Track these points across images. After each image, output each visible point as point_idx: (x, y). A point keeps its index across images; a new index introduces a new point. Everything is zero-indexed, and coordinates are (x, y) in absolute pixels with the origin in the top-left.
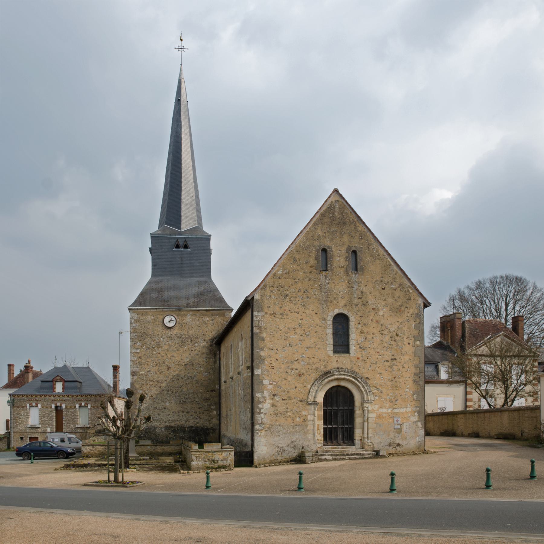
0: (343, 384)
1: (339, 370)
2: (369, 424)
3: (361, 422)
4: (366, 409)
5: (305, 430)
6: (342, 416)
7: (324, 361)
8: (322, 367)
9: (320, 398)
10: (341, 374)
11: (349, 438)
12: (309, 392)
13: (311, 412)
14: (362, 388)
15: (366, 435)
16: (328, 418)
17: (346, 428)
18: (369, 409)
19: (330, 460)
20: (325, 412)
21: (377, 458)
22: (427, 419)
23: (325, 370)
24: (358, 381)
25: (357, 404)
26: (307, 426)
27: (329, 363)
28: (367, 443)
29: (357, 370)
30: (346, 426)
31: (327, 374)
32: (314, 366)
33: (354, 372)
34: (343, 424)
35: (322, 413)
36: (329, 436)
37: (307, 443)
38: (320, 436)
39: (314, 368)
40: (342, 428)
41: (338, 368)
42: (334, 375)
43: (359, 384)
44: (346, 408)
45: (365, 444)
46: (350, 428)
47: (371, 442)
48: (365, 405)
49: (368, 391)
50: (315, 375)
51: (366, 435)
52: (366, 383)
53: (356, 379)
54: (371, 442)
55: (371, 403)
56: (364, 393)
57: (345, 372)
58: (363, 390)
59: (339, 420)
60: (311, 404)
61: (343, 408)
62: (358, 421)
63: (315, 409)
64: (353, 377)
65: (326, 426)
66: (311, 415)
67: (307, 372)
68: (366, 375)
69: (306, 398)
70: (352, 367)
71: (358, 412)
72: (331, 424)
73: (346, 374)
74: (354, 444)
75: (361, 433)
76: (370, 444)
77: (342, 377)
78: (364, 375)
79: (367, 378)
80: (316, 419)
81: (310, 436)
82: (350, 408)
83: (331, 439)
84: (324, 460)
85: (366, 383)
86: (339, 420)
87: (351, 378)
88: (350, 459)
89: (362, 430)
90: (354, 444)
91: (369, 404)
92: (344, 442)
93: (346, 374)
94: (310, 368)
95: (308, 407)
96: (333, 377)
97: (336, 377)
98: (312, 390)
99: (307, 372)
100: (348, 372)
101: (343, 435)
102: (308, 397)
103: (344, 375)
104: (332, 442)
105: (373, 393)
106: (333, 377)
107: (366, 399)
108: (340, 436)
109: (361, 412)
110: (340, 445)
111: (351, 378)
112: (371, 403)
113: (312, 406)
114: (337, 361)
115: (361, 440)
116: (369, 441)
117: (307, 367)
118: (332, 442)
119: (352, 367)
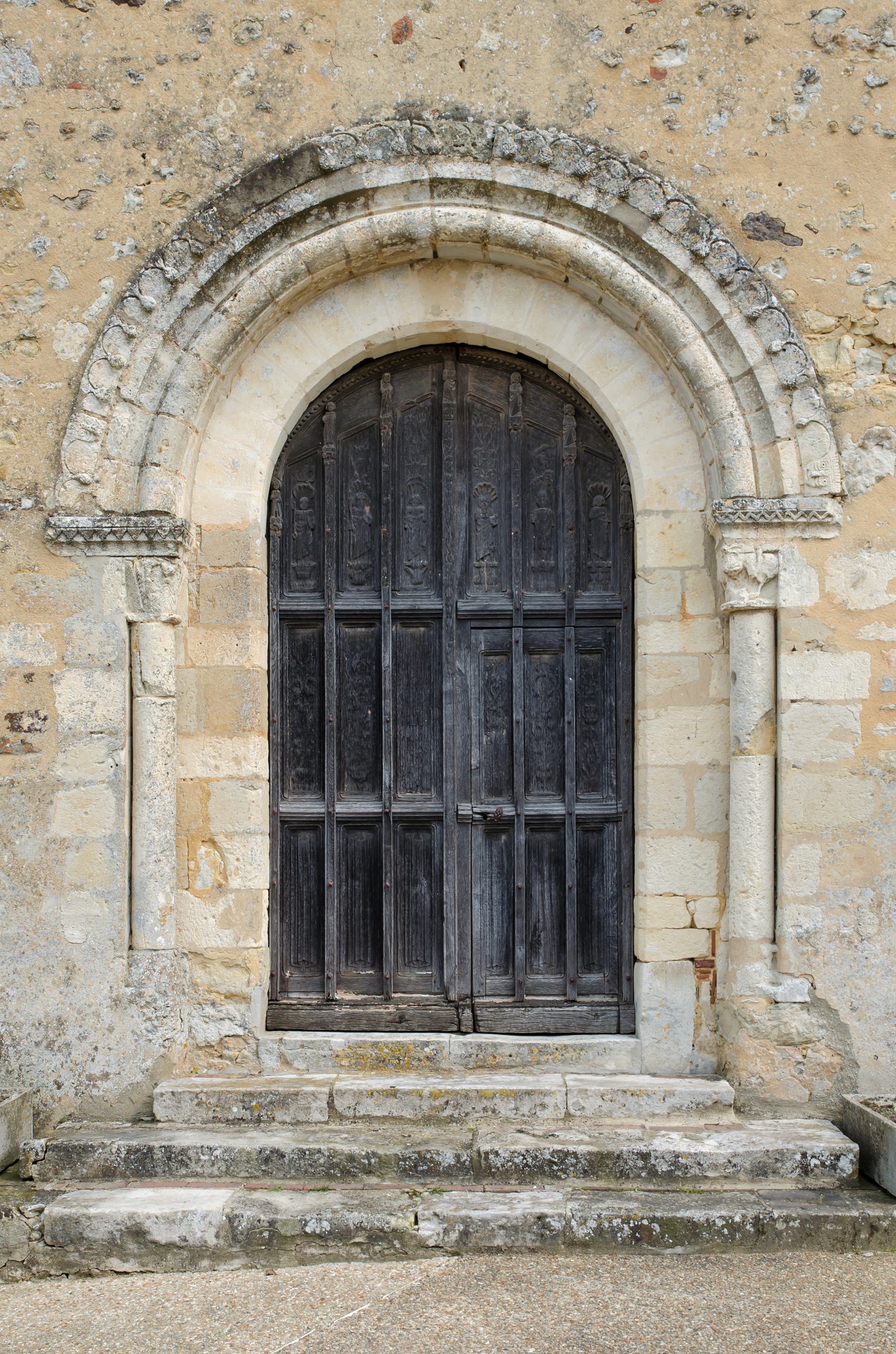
0: (492, 312)
1: (413, 131)
2: (789, 780)
3: (702, 753)
4: (743, 595)
5: (28, 848)
6: (499, 696)
7: (248, 34)
8: (227, 110)
9: (228, 476)
10: (440, 187)
11: (576, 933)
12: (74, 407)
13: (100, 637)
14: (698, 352)
15: (751, 916)
16: (326, 706)
17: (539, 824)
18: (789, 597)
19: (191, 1255)
20: (299, 644)
21: (853, 1237)
22: (482, 1029)
23: (260, 144)
24: (654, 261)
25: (660, 544)
26: (43, 792)
27: (310, 56)
28: (758, 1010)
29: (638, 134)
30: (535, 807)
31: (277, 187)
32: (135, 104)
33: (598, 159)
34: (501, 786)
35: (253, 650)
36: (349, 912)
37: (48, 1001)
38: (224, 909)
39: (126, 121)
40: (495, 827)
41: (409, 113)
42: (353, 199)
43: (664, 304)
44: (541, 598)
45: (741, 1019)
46: (591, 827)
47: (815, 1003)
48: (742, 550)
49: (768, 380)
50: (136, 208)
51: (751, 916)
52: (742, 279)
53: (629, 242)
54: (815, 1003)
55: (814, 520)
56: (726, 400)
57: (489, 151)
58: (713, 371)
59: (466, 731)
60: (94, 539)
61: (501, 603)
62: (666, 739)
63: (142, 599)
64: (598, 223)
65: (305, 806)
66: (90, 664)
67: (49, 169)
68: (749, 192)
69: (36, 468)
70: (580, 103)
71: (662, 640)
72: (370, 782)
73: (508, 175)
74: (625, 1024)
75: (709, 885)
76: (799, 1022)
77: (462, 215)
78: (729, 185)
79: (766, 228)
80: (153, 718)
81: (82, 918)
82: (590, 599)
83: (367, 941)
84: (113, 1247)
85: (742, 279)
86: (466, 731)
87: (566, 237)
88: (467, 1240)
89: (712, 849)
90: (625, 1024)
91: (783, 540)
92: (517, 993)
93: (508, 175)
94: (88, 122)
95: (65, 574)
96: (353, 229)
97: (387, 218)
98: (101, 378)
99: (49, 169)
100: (526, 155)
101: (510, 904)
102: (56, 462)
103: (485, 190)
104: (382, 988)
105: (835, 411)
106: (353, 229)
107: (744, 480)
108: (472, 907)
109: (700, 636)
110: (463, 1016)
111: (566, 237)
112: (814, 520)
113: (109, 571)
114: (402, 32)
115: (703, 966)
116: (794, 989)
117: (49, 110)
118: (382, 988)
119: (580, 103)
